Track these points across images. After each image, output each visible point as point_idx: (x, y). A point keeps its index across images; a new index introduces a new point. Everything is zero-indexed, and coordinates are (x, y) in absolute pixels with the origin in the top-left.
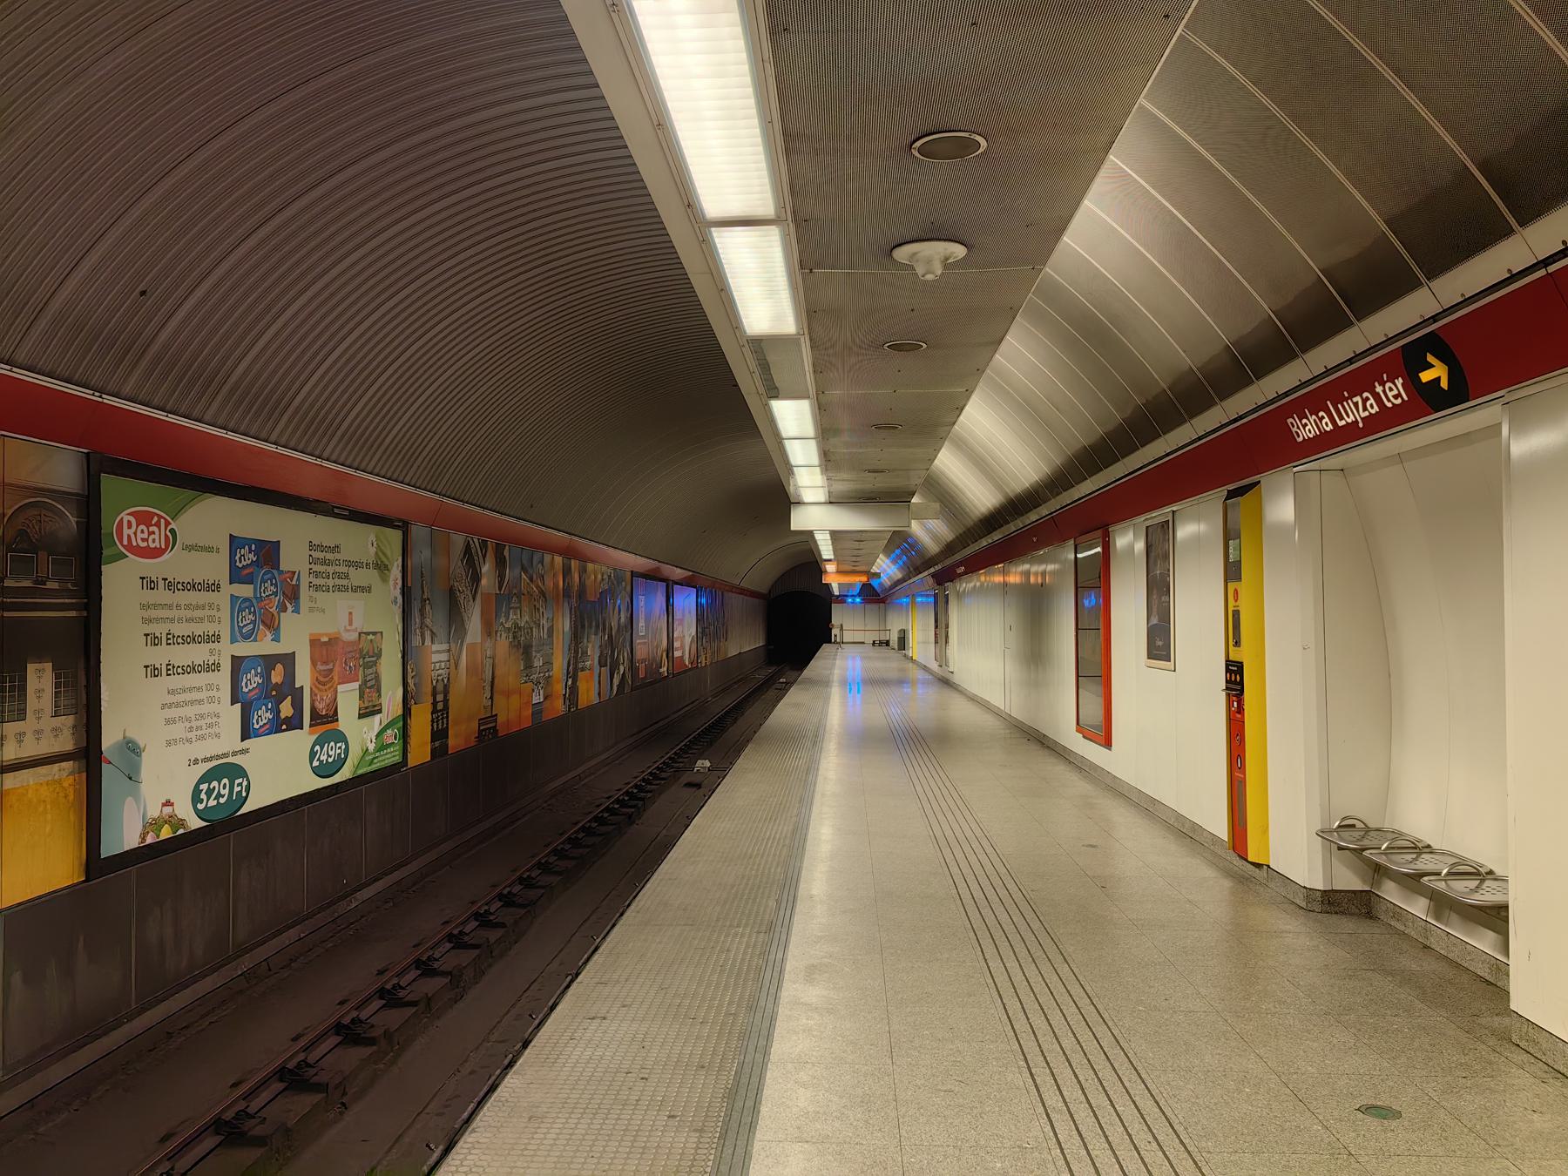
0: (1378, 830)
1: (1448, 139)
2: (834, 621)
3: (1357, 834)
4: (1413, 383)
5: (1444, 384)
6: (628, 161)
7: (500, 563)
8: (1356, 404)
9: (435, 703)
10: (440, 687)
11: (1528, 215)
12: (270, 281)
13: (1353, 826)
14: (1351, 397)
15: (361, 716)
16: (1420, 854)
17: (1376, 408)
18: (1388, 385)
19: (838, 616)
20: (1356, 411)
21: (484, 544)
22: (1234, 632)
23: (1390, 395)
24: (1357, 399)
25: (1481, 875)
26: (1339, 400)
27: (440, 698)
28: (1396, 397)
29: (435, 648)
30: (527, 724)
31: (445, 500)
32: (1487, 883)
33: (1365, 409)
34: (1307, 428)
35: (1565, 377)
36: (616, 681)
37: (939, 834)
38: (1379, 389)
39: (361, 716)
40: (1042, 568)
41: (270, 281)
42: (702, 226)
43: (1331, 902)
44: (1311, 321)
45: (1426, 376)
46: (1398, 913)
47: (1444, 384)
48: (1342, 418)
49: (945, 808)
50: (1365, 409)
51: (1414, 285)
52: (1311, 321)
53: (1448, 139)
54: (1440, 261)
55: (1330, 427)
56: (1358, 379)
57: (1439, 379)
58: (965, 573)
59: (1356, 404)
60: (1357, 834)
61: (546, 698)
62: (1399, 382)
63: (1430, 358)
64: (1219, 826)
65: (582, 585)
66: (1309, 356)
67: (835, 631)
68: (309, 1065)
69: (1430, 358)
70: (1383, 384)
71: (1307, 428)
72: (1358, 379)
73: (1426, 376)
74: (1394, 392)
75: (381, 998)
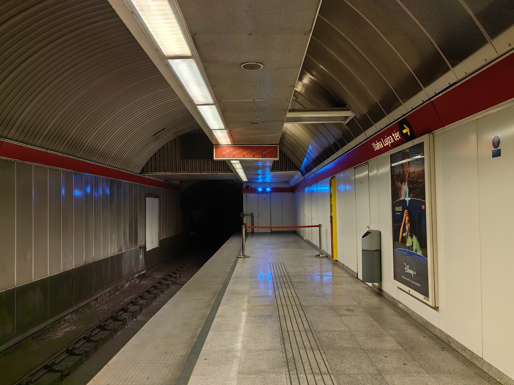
2: (246, 209)
4: (401, 134)
5: (409, 134)
11: (495, 32)
15: (494, 156)
19: (250, 204)
21: (416, 251)
22: (331, 211)
24: (388, 138)
28: (398, 137)
34: (378, 146)
37: (292, 290)
38: (393, 135)
39: (494, 156)
40: (108, 290)
45: (404, 131)
47: (409, 134)
51: (384, 116)
55: (382, 147)
57: (407, 133)
62: (398, 133)
63: (405, 126)
64: (330, 254)
67: (246, 220)
69: (405, 126)
71: (378, 146)
73: (404, 131)
74: (397, 136)
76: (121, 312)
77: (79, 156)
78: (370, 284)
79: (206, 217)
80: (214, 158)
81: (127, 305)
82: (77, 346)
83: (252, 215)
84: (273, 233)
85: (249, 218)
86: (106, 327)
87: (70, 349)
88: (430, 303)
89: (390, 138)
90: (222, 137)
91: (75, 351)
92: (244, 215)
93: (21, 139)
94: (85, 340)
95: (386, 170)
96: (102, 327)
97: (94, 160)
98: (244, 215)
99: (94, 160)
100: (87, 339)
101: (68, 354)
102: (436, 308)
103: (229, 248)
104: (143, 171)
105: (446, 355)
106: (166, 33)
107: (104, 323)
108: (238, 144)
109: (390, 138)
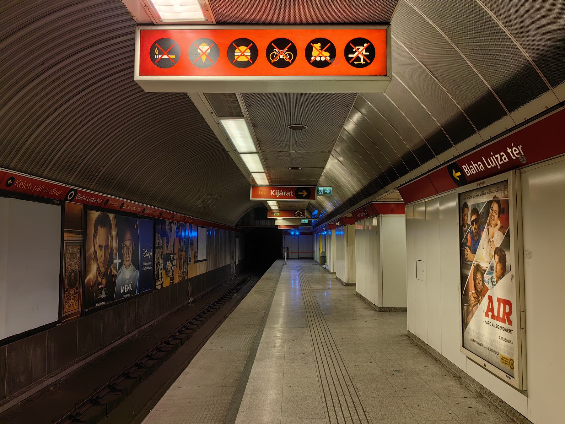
1: (437, 122)
5: (454, 171)
6: (128, 17)
12: (78, 146)
18: (514, 149)
23: (515, 153)
24: (498, 156)
26: (488, 156)
28: (517, 154)
33: (501, 160)
35: (564, 158)
38: (509, 151)
41: (78, 146)
42: (238, 154)
44: (483, 111)
45: (459, 174)
47: (454, 171)
48: (489, 165)
50: (501, 160)
53: (437, 122)
54: (482, 125)
56: (499, 145)
58: (341, 225)
59: (497, 158)
62: (520, 147)
63: (458, 179)
65: (468, 243)
66: (439, 157)
68: (80, 414)
69: (458, 179)
70: (511, 148)
71: (470, 170)
72: (499, 145)
73: (459, 174)
75: (70, 419)
76: (164, 345)
77: (91, 188)
78: (172, 57)
79: (260, 248)
80: (251, 199)
81: (141, 360)
83: (288, 248)
84: (300, 258)
85: (286, 250)
88: (513, 382)
89: (501, 156)
90: (261, 179)
92: (283, 248)
93: (88, 187)
95: (454, 204)
97: (70, 181)
98: (283, 248)
99: (70, 181)
102: (524, 392)
104: (236, 225)
105: (423, 359)
108: (275, 184)
109: (501, 156)
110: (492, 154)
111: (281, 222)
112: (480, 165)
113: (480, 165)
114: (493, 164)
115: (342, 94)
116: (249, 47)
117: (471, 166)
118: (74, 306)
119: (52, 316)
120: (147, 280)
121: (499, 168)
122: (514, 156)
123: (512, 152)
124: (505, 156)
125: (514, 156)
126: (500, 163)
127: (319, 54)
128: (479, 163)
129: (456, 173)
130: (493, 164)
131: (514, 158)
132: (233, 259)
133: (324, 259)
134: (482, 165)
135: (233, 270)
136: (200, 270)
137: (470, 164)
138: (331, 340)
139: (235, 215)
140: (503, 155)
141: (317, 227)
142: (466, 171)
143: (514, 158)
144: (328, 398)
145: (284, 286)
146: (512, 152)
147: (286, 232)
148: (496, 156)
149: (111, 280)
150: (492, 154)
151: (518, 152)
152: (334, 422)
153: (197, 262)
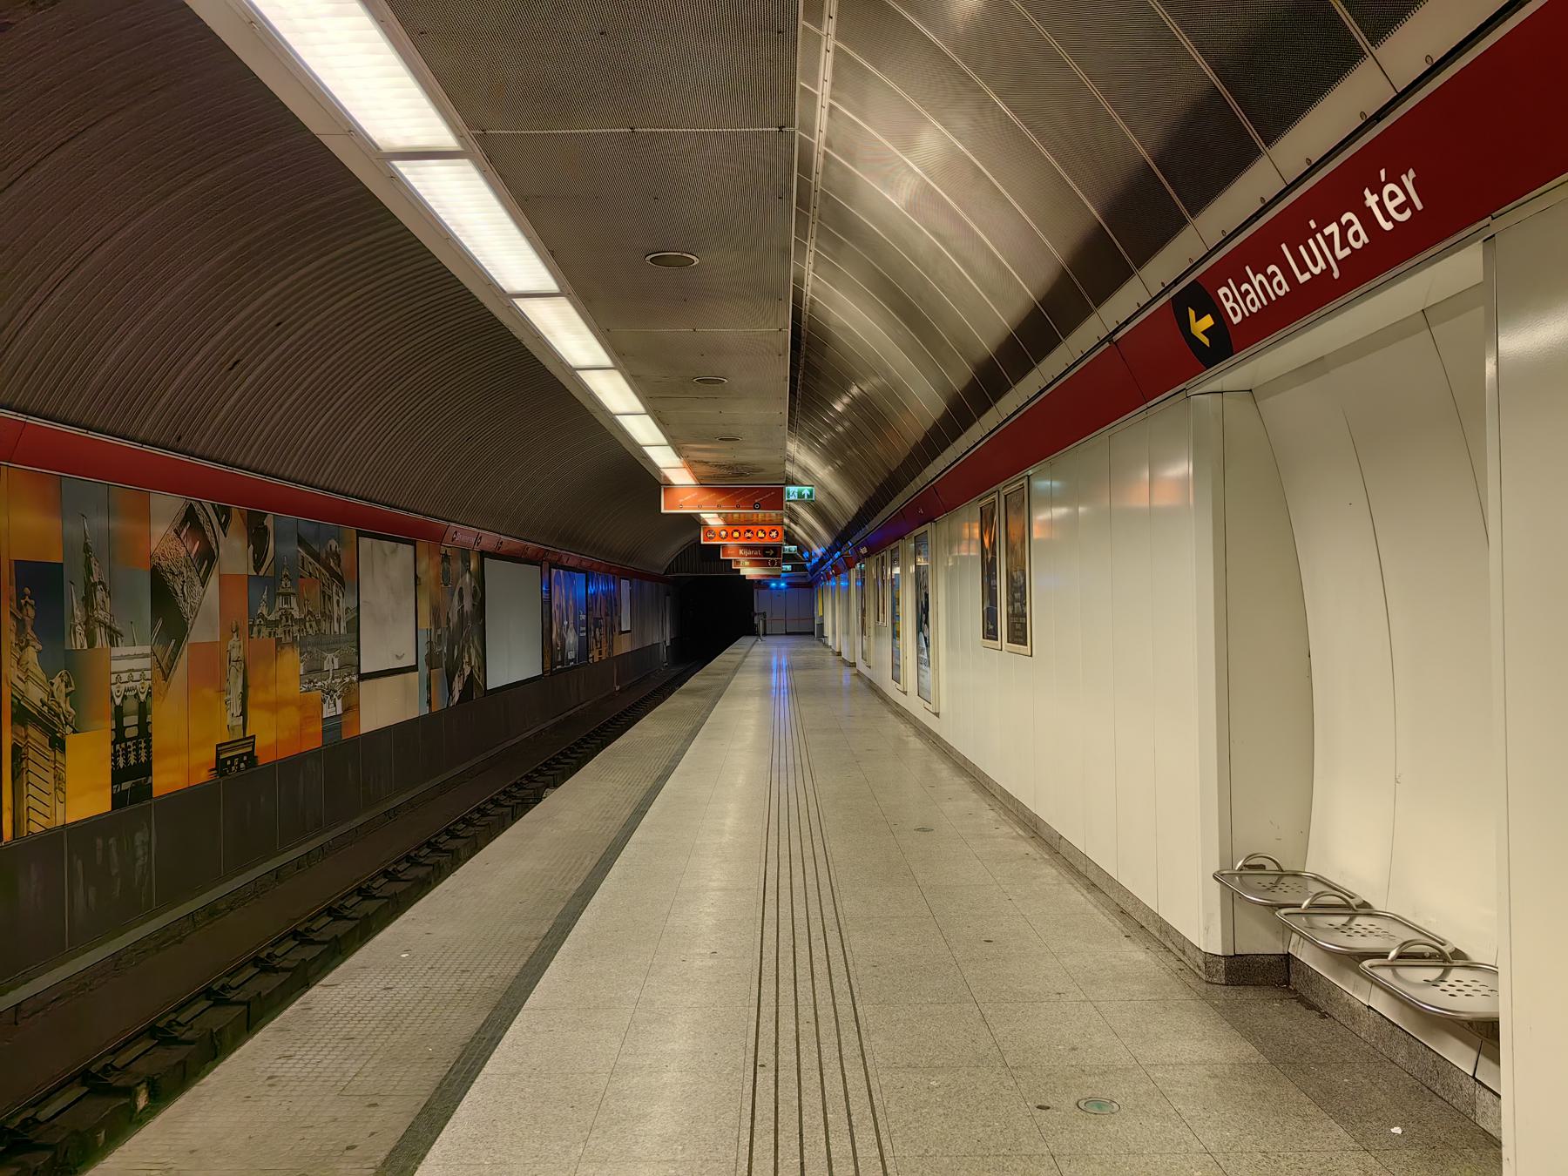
0: (1296, 875)
3: (1267, 881)
5: (1192, 313)
7: (257, 536)
8: (1329, 240)
9: (119, 731)
10: (131, 705)
13: (1262, 867)
14: (1320, 229)
16: (1353, 916)
17: (1364, 237)
20: (1329, 246)
23: (1390, 206)
24: (1333, 228)
25: (1447, 959)
26: (1300, 236)
27: (131, 720)
28: (1408, 203)
29: (116, 652)
30: (316, 744)
31: (33, 420)
32: (1455, 974)
33: (1344, 244)
36: (458, 686)
38: (1371, 200)
43: (1242, 972)
45: (1208, 321)
46: (1355, 1013)
47: (1192, 313)
48: (1304, 268)
49: (808, 852)
50: (1344, 244)
52: (1205, 152)
56: (1338, 188)
59: (1329, 240)
60: (1267, 881)
61: (346, 710)
62: (1408, 180)
63: (1206, 341)
69: (1206, 341)
70: (1377, 190)
73: (1208, 321)
76: (426, 851)
79: (708, 612)
82: (234, 982)
86: (312, 936)
87: (94, 1069)
89: (1344, 229)
91: (110, 1080)
94: (83, 1084)
96: (300, 934)
100: (161, 1035)
101: (85, 1089)
103: (745, 642)
106: (376, 93)
107: (270, 950)
110: (1313, 224)
111: (749, 571)
112: (1274, 274)
113: (1274, 274)
114: (1315, 264)
115: (272, 96)
116: (1133, 267)
117: (1245, 286)
118: (548, 666)
119: (537, 671)
120: (584, 648)
121: (1336, 275)
122: (1388, 217)
123: (1381, 204)
124: (1357, 226)
125: (1388, 217)
126: (1341, 254)
127: (761, 534)
128: (1272, 268)
129: (1197, 319)
130: (1315, 264)
131: (1388, 226)
132: (661, 635)
133: (821, 626)
134: (1280, 277)
135: (663, 652)
136: (624, 646)
137: (1242, 279)
138: (813, 809)
139: (666, 554)
140: (1350, 223)
141: (809, 580)
142: (1228, 305)
143: (1388, 226)
144: (765, 1079)
145: (721, 777)
146: (1381, 204)
147: (760, 584)
148: (1327, 231)
149: (563, 640)
150: (1313, 224)
151: (1401, 198)
152: (763, 1167)
153: (622, 632)
